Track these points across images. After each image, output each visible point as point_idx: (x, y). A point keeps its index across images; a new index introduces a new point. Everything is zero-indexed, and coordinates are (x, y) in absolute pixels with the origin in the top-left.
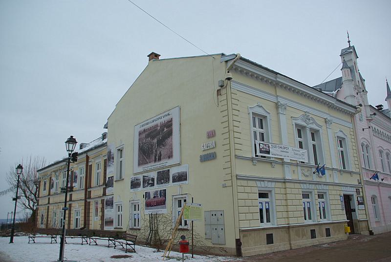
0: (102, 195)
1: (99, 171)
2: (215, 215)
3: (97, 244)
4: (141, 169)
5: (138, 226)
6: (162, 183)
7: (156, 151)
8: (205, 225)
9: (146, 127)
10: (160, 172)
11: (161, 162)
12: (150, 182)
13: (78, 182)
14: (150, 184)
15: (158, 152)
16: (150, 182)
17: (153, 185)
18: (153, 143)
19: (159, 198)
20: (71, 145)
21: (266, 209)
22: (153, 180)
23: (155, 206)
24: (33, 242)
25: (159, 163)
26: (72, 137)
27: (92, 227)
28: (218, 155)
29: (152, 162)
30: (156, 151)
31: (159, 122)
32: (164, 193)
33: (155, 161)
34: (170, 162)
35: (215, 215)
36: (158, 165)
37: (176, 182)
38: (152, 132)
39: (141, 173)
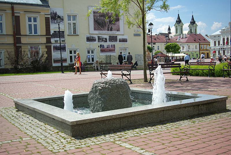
3: (170, 151)
6: (112, 42)
15: (110, 27)
16: (104, 40)
17: (106, 41)
21: (124, 57)
22: (106, 39)
33: (108, 30)
34: (118, 33)
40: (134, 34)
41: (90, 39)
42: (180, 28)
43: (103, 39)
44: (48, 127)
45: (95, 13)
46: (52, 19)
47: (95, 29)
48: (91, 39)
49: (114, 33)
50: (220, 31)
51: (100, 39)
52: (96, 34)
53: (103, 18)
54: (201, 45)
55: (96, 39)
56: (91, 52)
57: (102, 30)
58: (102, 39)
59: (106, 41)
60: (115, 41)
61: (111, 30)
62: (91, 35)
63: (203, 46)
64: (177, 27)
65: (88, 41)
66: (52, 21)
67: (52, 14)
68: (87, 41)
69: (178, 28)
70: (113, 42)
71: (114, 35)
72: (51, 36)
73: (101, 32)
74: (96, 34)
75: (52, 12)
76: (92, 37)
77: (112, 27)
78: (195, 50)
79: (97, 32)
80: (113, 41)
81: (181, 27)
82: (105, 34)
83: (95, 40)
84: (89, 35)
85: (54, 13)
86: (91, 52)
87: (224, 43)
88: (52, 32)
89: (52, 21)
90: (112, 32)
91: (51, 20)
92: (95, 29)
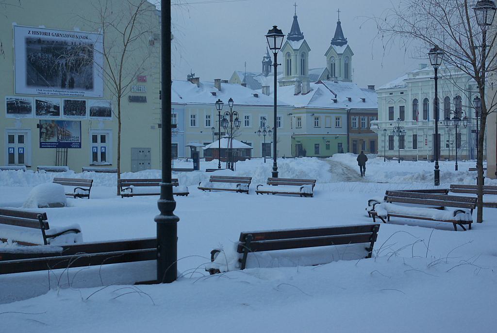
2: (143, 152)
3: (154, 305)
5: (415, 147)
6: (73, 114)
8: (132, 160)
10: (70, 101)
12: (52, 110)
14: (49, 112)
15: (68, 78)
16: (52, 110)
17: (57, 114)
21: (102, 153)
22: (57, 108)
24: (265, 88)
27: (475, 183)
29: (57, 86)
33: (63, 86)
34: (87, 93)
35: (143, 152)
37: (95, 116)
40: (130, 97)
41: (16, 108)
42: (299, 58)
43: (49, 107)
44: (161, 27)
45: (30, 42)
47: (29, 83)
48: (18, 107)
49: (76, 94)
50: (406, 77)
51: (41, 107)
52: (31, 95)
53: (51, 56)
54: (352, 117)
55: (31, 107)
56: (16, 139)
57: (48, 86)
58: (47, 107)
59: (57, 114)
60: (80, 114)
61: (72, 86)
62: (20, 98)
63: (359, 119)
64: (289, 55)
65: (11, 113)
68: (8, 112)
69: (293, 58)
70: (76, 116)
71: (76, 99)
73: (44, 90)
74: (31, 95)
76: (21, 102)
77: (72, 79)
78: (338, 132)
79: (34, 90)
80: (74, 112)
81: (303, 56)
82: (56, 96)
83: (27, 111)
84: (14, 98)
86: (16, 139)
87: (415, 112)
90: (74, 90)
92: (29, 83)
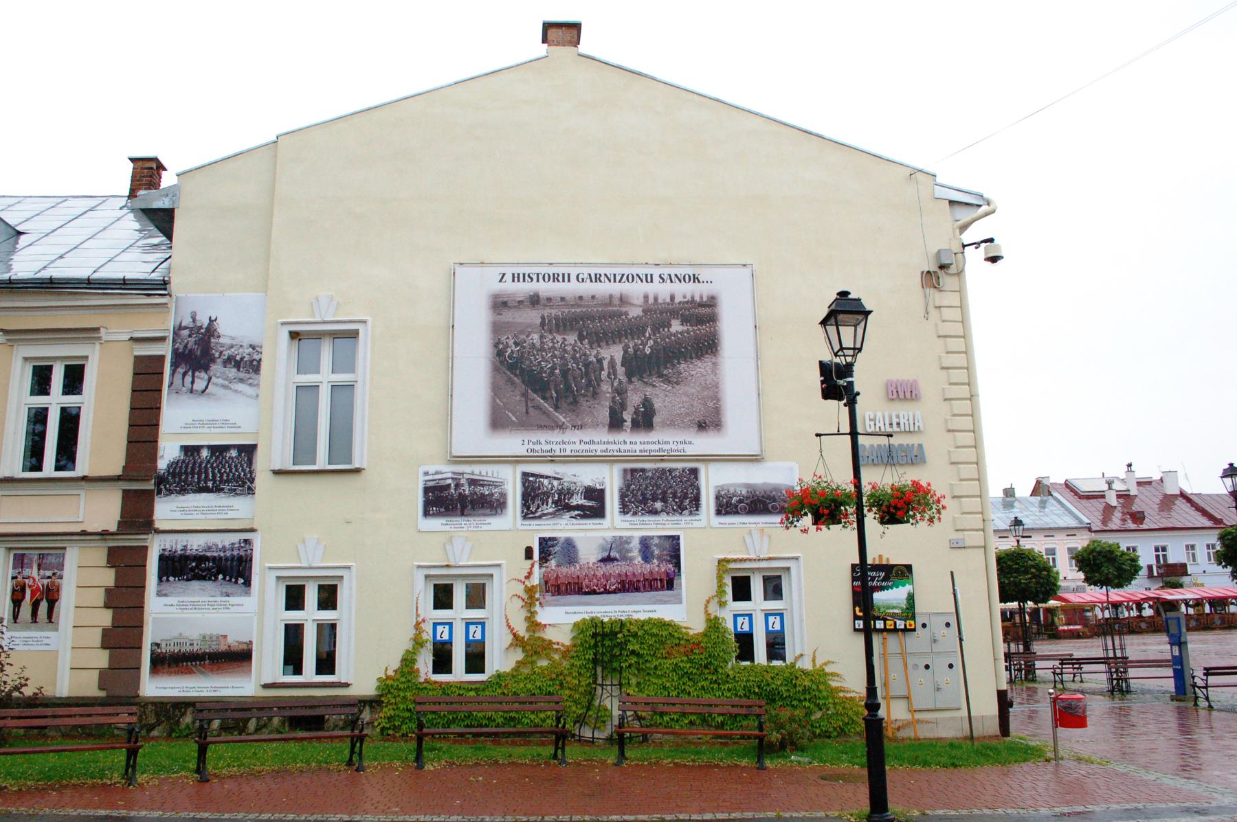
0: (113, 527)
1: (543, 442)
4: (513, 443)
6: (655, 512)
7: (620, 391)
9: (545, 288)
10: (643, 470)
11: (653, 436)
13: (1117, 541)
14: (569, 508)
18: (600, 361)
19: (657, 567)
20: (847, 333)
23: (614, 592)
25: (611, 438)
26: (843, 294)
28: (929, 453)
30: (620, 391)
31: (636, 290)
32: (673, 549)
33: (615, 423)
34: (702, 444)
36: (632, 443)
38: (591, 318)
39: (516, 460)
46: (181, 370)
66: (178, 377)
67: (186, 333)
72: (161, 480)
75: (187, 321)
85: (195, 329)
88: (168, 452)
89: (178, 377)
91: (173, 373)
